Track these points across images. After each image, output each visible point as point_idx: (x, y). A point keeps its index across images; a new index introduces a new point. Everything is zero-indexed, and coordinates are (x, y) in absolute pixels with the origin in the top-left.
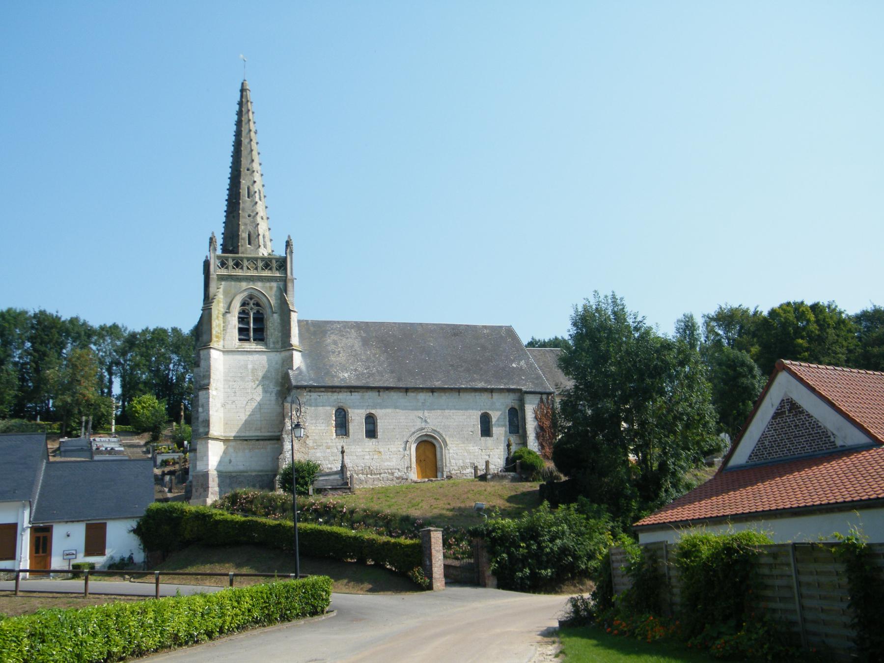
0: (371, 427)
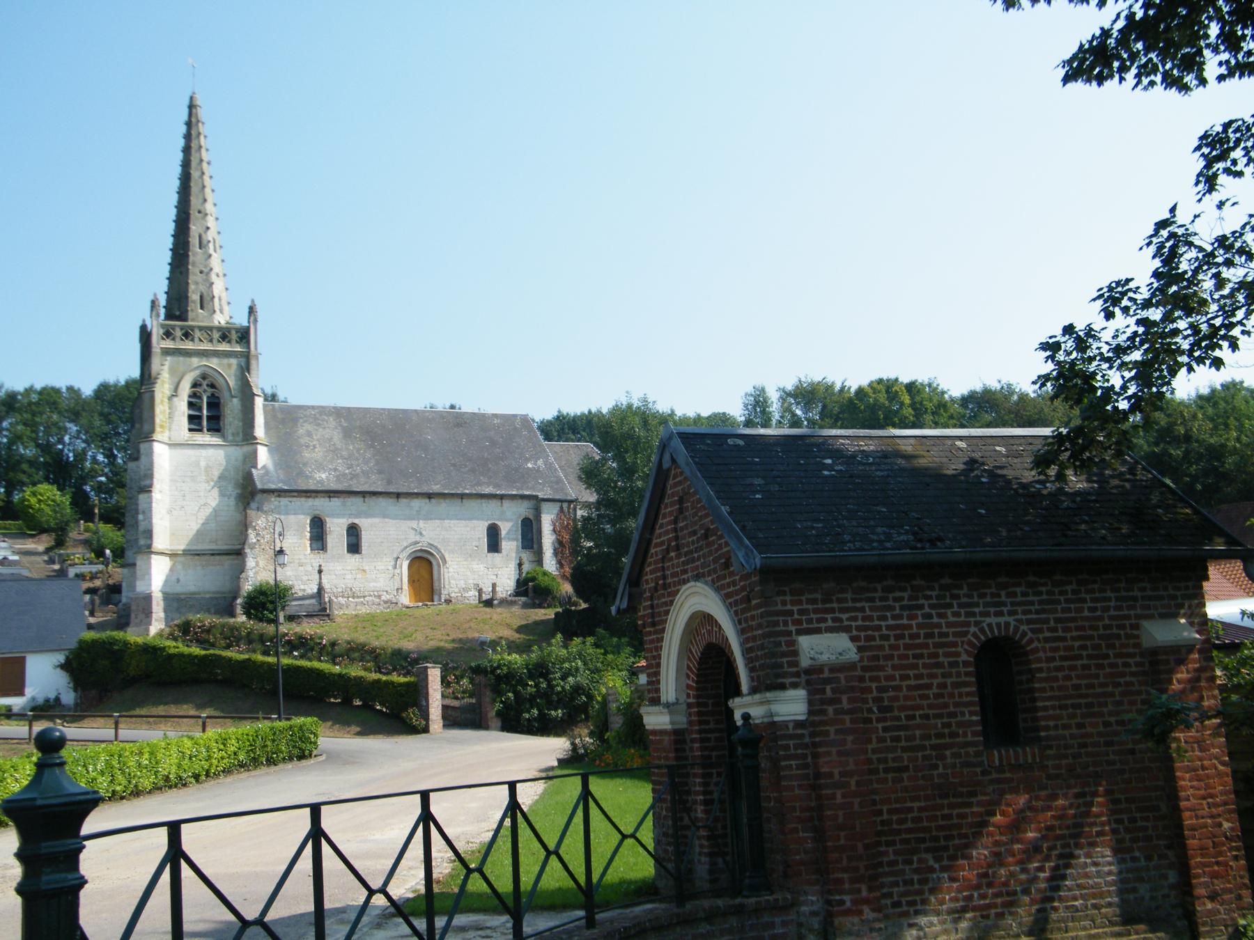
0: (354, 540)
